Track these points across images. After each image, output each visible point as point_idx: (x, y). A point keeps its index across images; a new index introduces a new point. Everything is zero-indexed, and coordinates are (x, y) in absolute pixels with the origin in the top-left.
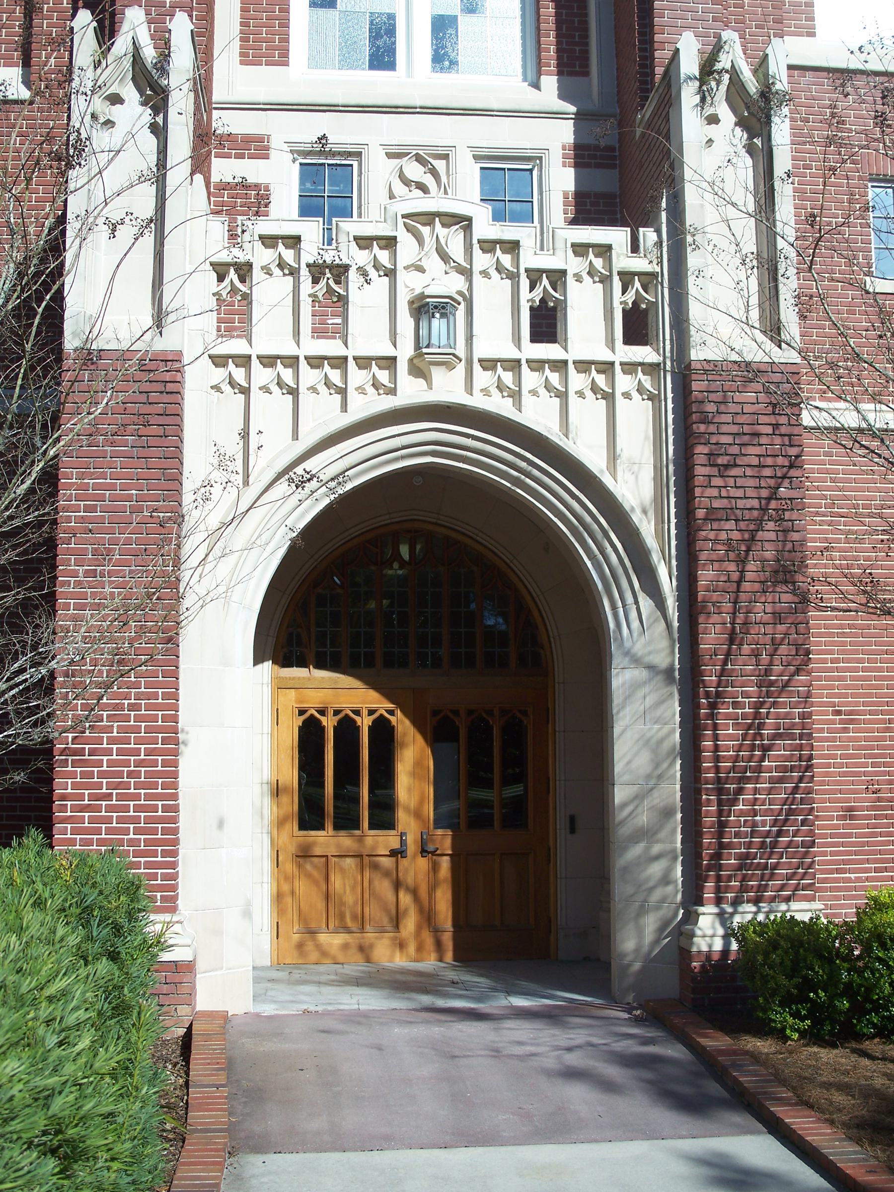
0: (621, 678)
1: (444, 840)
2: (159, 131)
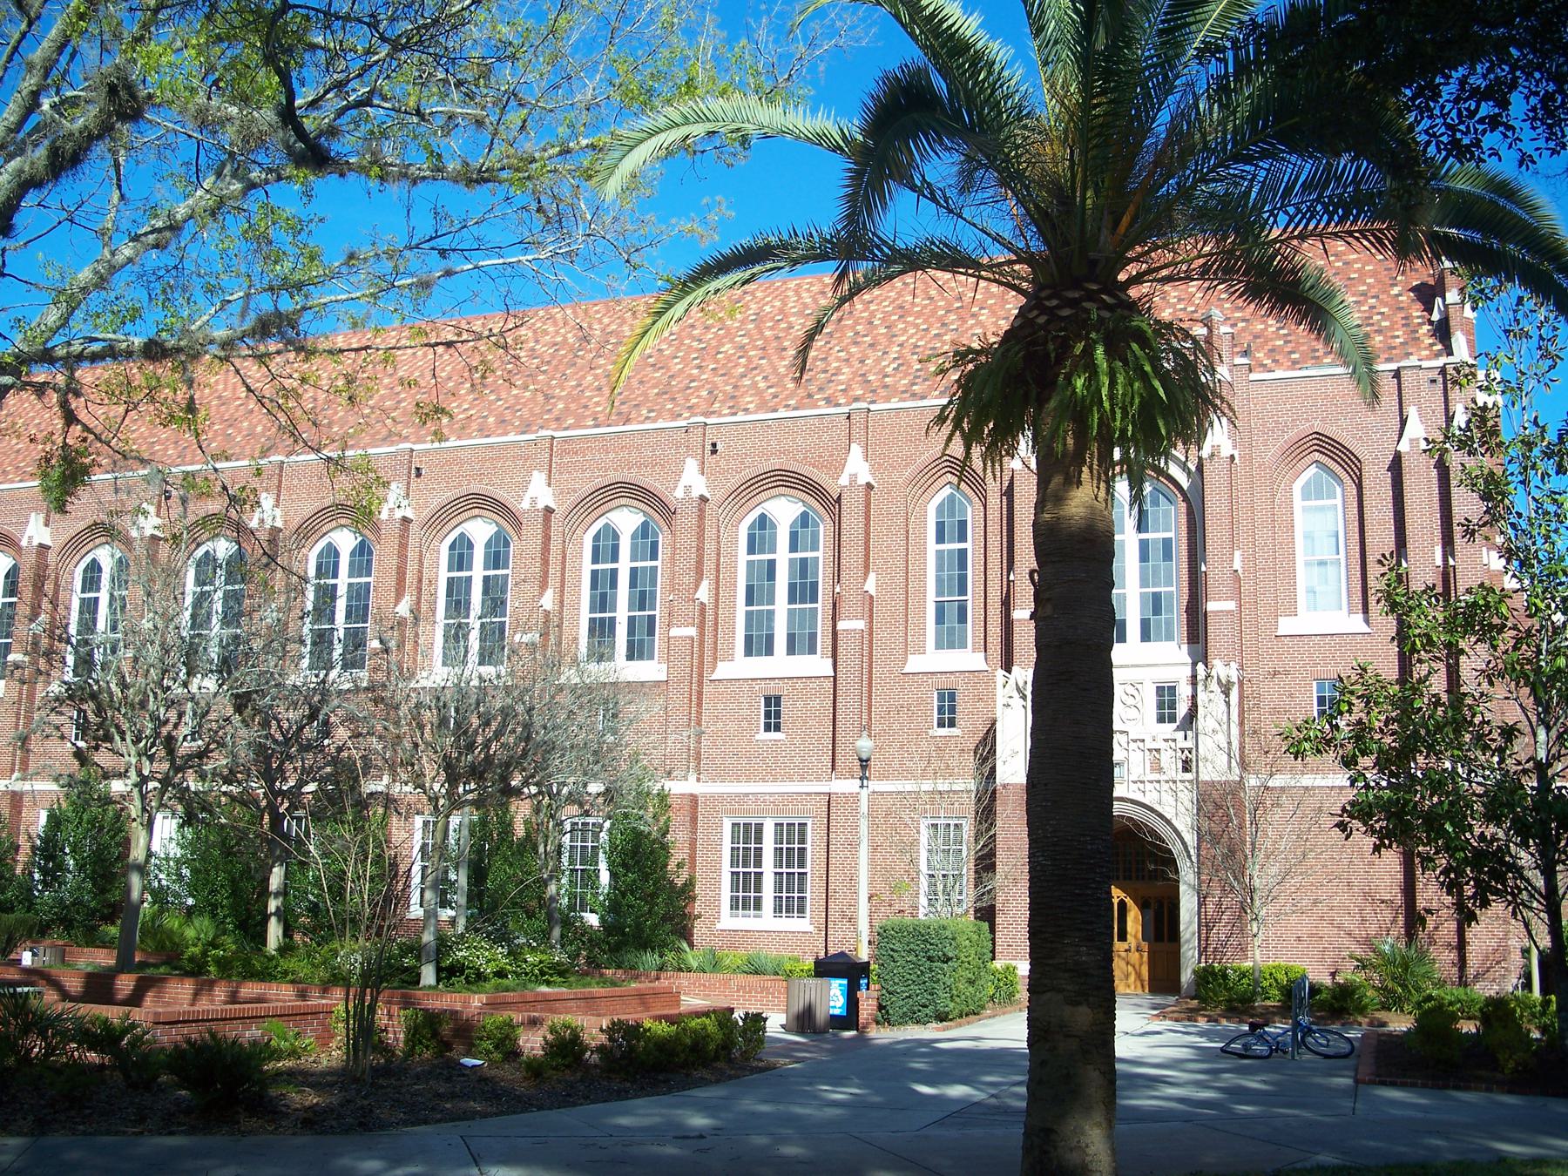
0: (1182, 888)
1: (1145, 946)
2: (1228, 704)
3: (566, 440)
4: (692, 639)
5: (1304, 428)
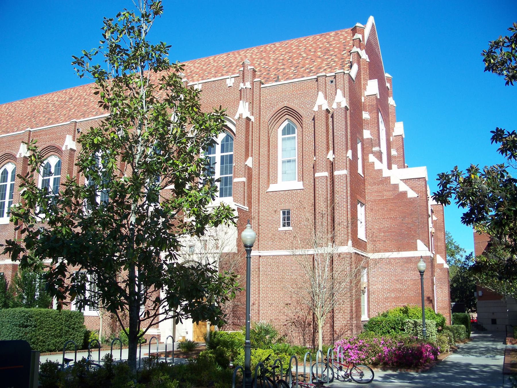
3: (35, 132)
4: (244, 182)
5: (281, 105)
